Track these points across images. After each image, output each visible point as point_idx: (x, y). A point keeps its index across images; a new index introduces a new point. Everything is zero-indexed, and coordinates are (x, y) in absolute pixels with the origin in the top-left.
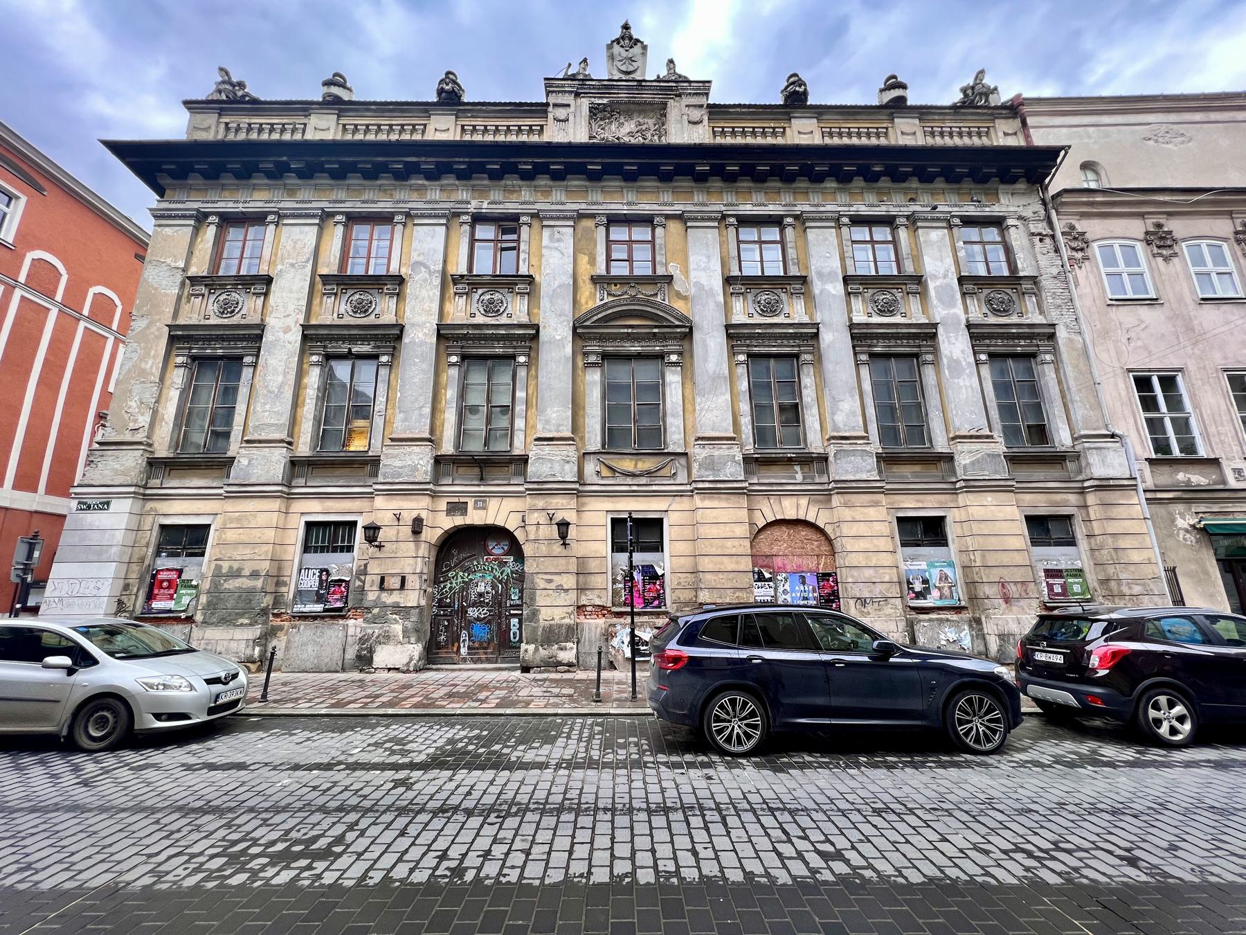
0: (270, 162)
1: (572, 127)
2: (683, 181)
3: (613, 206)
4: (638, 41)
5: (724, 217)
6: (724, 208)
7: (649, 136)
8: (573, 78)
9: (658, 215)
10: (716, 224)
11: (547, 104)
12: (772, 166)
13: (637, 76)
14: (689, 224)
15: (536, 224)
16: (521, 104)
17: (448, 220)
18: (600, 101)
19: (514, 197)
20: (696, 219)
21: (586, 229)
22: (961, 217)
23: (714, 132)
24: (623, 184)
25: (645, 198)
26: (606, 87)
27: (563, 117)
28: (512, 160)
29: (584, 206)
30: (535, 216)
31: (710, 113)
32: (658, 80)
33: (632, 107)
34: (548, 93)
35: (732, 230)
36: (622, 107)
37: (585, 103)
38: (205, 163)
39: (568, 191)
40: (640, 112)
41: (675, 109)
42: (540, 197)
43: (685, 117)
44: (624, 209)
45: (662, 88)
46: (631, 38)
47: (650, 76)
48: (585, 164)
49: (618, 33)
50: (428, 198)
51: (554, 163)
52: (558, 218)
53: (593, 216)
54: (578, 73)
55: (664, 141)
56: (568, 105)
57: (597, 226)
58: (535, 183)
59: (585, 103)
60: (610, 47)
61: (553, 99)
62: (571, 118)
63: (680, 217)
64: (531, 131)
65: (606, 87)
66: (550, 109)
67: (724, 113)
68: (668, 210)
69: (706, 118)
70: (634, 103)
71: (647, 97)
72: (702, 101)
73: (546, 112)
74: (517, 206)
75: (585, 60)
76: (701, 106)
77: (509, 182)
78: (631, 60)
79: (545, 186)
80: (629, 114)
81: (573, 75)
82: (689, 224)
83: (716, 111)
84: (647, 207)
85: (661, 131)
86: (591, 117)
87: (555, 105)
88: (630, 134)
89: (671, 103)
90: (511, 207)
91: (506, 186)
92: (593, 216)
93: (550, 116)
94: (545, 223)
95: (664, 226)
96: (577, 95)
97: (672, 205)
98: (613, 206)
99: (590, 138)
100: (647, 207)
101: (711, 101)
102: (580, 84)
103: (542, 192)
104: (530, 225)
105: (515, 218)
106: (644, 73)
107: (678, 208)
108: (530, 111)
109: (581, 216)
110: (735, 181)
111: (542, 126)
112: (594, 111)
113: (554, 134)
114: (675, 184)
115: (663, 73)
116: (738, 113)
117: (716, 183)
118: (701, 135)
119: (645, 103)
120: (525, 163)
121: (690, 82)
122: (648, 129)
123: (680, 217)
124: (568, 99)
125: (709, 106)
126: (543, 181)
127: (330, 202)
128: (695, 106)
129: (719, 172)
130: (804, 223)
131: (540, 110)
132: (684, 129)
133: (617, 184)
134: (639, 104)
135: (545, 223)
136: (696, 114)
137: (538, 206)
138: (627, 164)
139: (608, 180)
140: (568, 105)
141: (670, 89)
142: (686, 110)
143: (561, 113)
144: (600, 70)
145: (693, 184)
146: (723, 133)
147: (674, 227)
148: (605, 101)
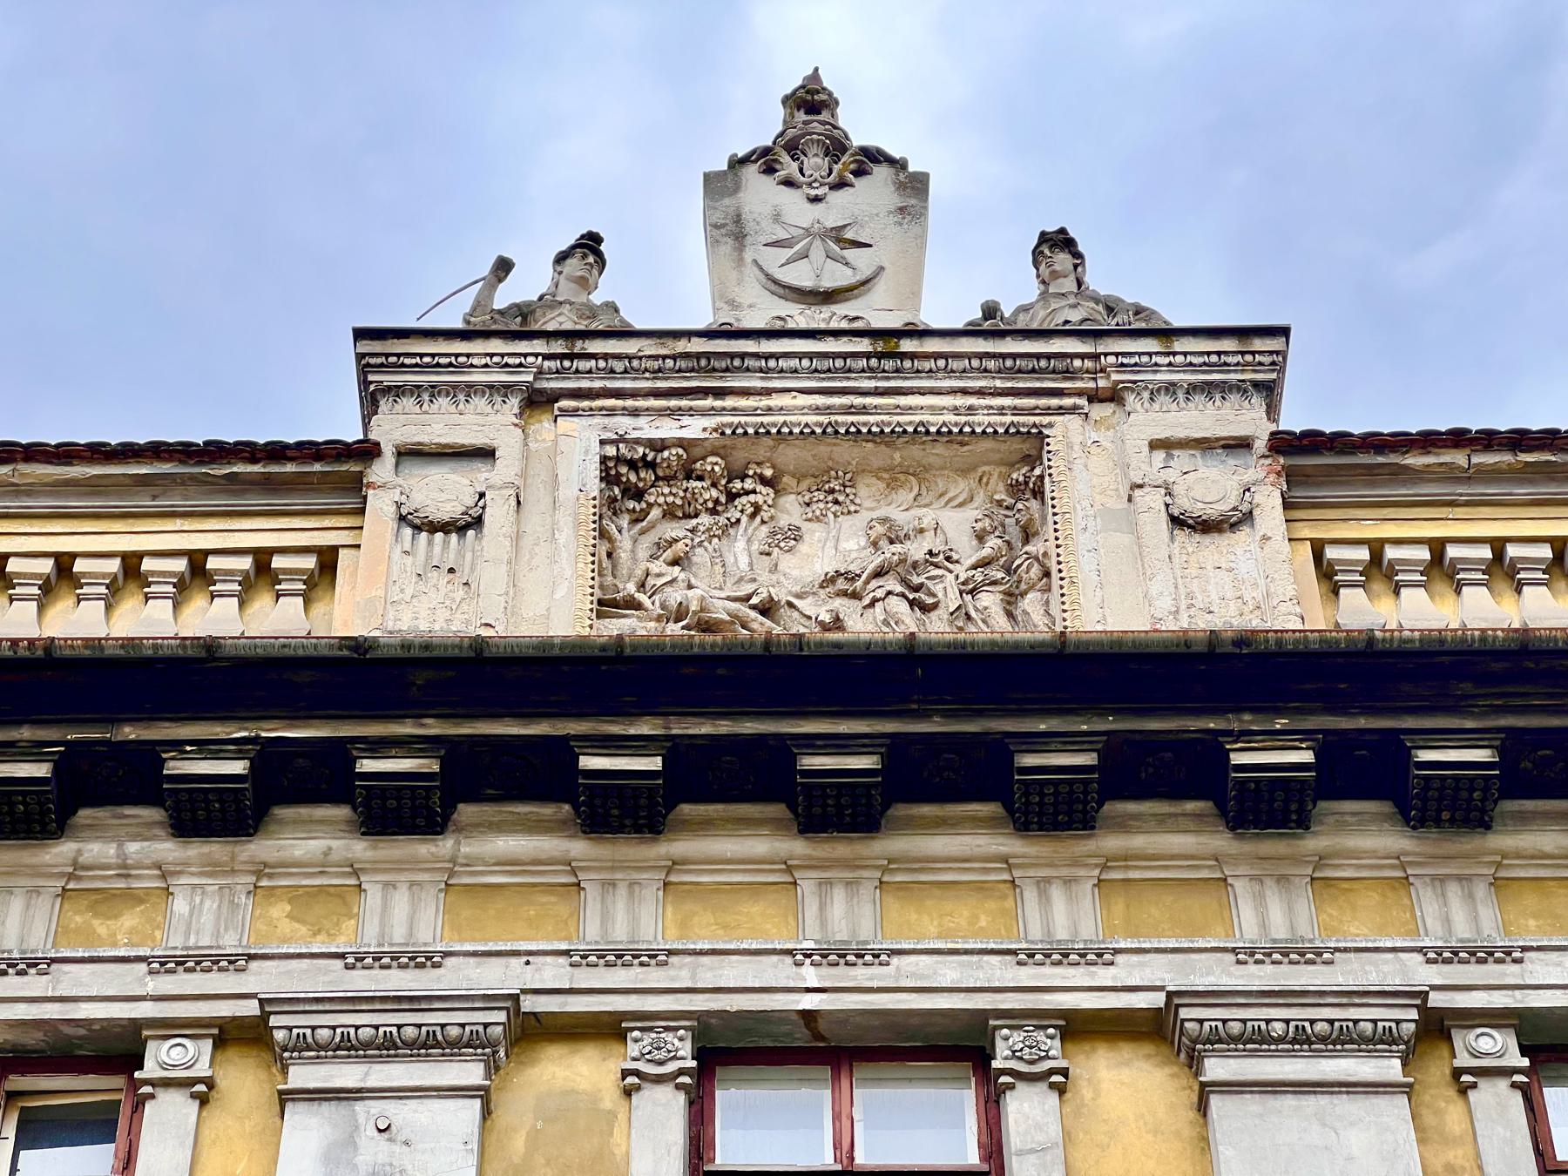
0: (33, 751)
1: (509, 557)
2: (1162, 823)
3: (733, 972)
4: (872, 157)
5: (1437, 1027)
6: (1424, 975)
7: (947, 591)
8: (521, 325)
9: (171, 1028)
10: (1390, 1068)
11: (367, 451)
12: (1329, 747)
13: (878, 311)
14: (1217, 1068)
15: (243, 1081)
16: (216, 451)
17: (493, 1067)
18: (666, 429)
19: (122, 930)
20: (1257, 1041)
21: (566, 1110)
22: (1522, 1023)
23: (1326, 572)
24: (797, 847)
25: (925, 923)
26: (702, 363)
27: (448, 509)
28: (130, 733)
29: (553, 973)
30: (240, 1036)
31: (1293, 477)
32: (990, 324)
33: (846, 452)
34: (370, 401)
35: (1498, 1105)
36: (789, 456)
37: (576, 445)
38: (238, 748)
39: (455, 886)
40: (893, 478)
41: (1092, 459)
42: (280, 924)
43: (1153, 500)
44: (798, 989)
45: (1010, 365)
46: (836, 146)
47: (946, 303)
48: (564, 750)
49: (766, 125)
50: (592, 934)
51: (379, 747)
52: (388, 1047)
53: (608, 1029)
54: (547, 302)
55: (1038, 621)
56: (486, 454)
57: (632, 1084)
58: (260, 848)
59: (576, 445)
60: (719, 185)
61: (396, 425)
62: (498, 515)
63: (1154, 1028)
64: (262, 570)
65: (707, 360)
66: (381, 470)
67: (1371, 474)
68: (1079, 988)
69: (1269, 502)
70: (855, 435)
71: (931, 406)
72: (1249, 419)
73: (356, 486)
74: (133, 979)
75: (590, 244)
76: (1241, 445)
77: (97, 850)
78: (841, 239)
79: (322, 865)
80: (832, 488)
81: (523, 311)
82: (1217, 1068)
83: (1316, 463)
84: (949, 972)
85: (1016, 563)
86: (612, 505)
87: (410, 454)
88: (842, 583)
89: (1065, 433)
90: (93, 994)
91: (77, 869)
92: (608, 1029)
93: (380, 505)
94: (302, 1076)
95: (1059, 1083)
96: (537, 401)
97: (1101, 956)
98: (733, 972)
99: (607, 606)
100: (949, 972)
101: (1294, 419)
102: (553, 348)
103: (303, 899)
104: (204, 1093)
105: (117, 1050)
106: (914, 295)
107: (1137, 979)
108: (268, 484)
109: (531, 1030)
110: (1303, 823)
111: (328, 560)
112: (627, 480)
113: (389, 595)
114: (1111, 843)
115: (1017, 289)
116: (1451, 475)
117: (1363, 836)
118: (1257, 586)
119: (921, 434)
120: (207, 748)
121: (1167, 333)
122: (941, 559)
123: (1154, 1028)
124: (488, 421)
125: (1283, 444)
126: (309, 839)
127: (580, 958)
128: (1204, 445)
129: (1366, 772)
130: (1194, 1063)
131: (331, 473)
132: (1145, 553)
133: (760, 845)
134: (879, 437)
135: (302, 1076)
136: (1211, 485)
137: (265, 980)
138: (815, 743)
139: (704, 826)
140: (486, 454)
141: (1062, 366)
142: (1153, 466)
143: (440, 492)
144: (669, 281)
145: (1220, 841)
146: (1379, 570)
147: (1125, 1083)
148: (694, 428)
